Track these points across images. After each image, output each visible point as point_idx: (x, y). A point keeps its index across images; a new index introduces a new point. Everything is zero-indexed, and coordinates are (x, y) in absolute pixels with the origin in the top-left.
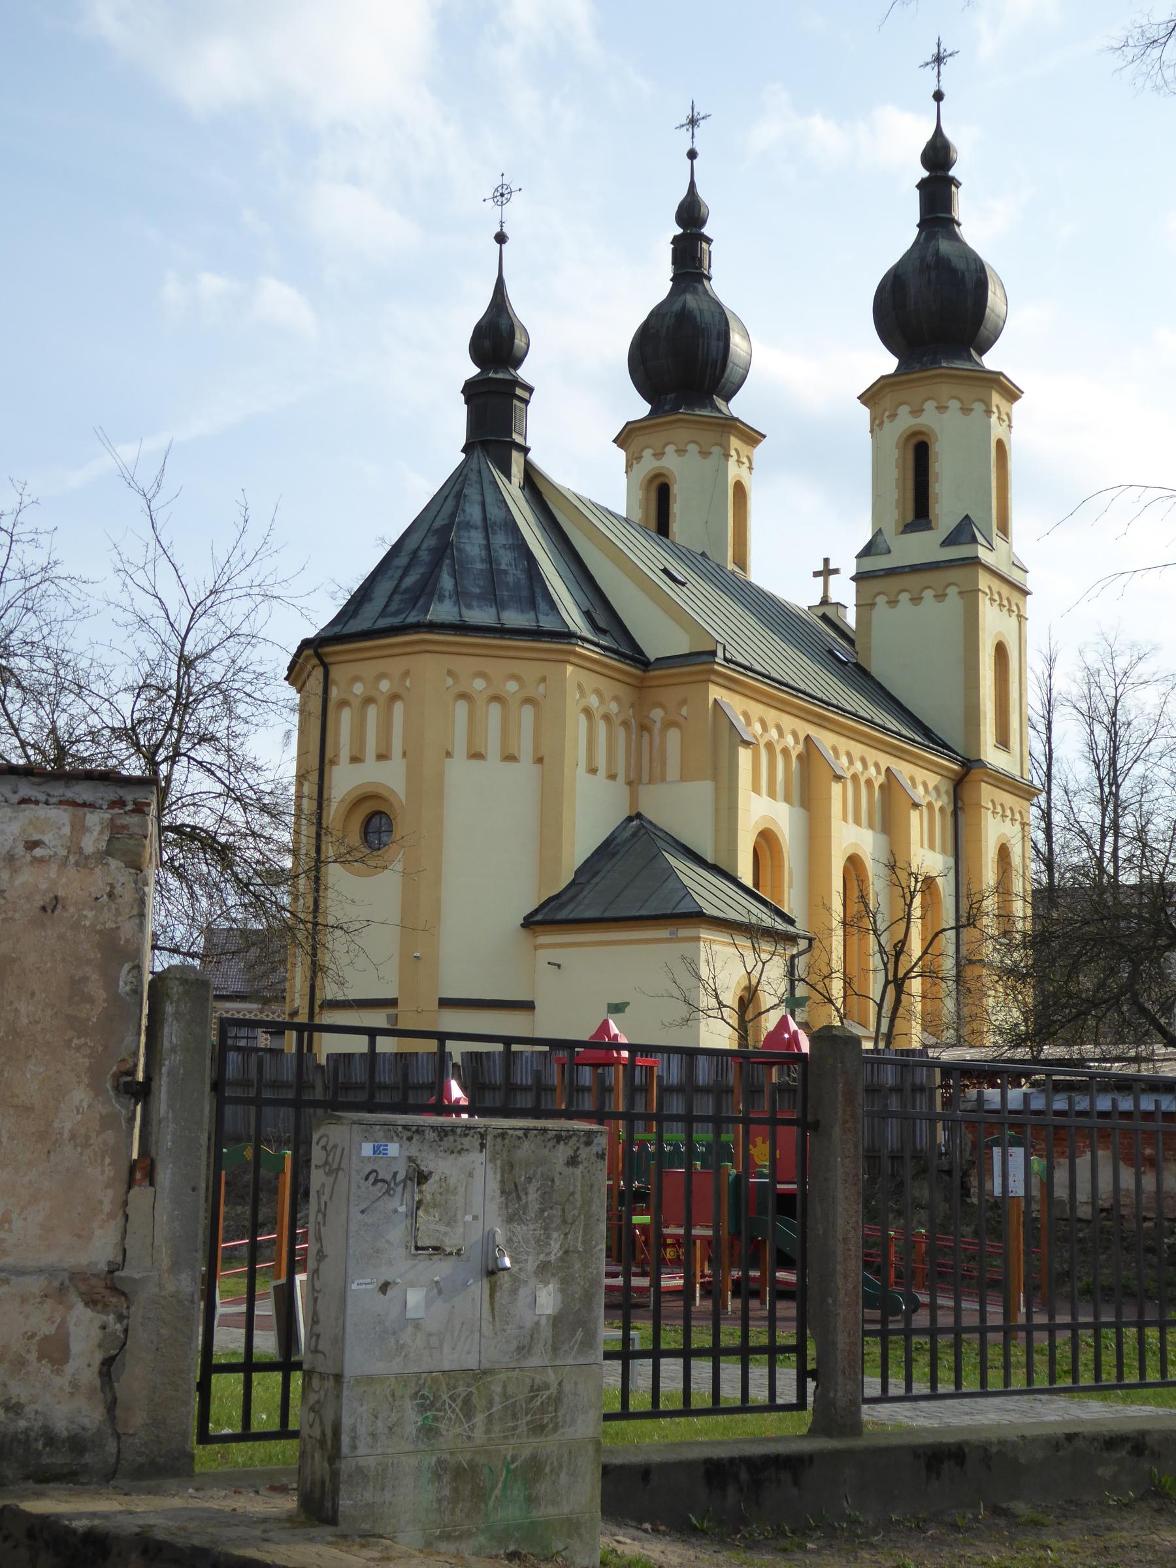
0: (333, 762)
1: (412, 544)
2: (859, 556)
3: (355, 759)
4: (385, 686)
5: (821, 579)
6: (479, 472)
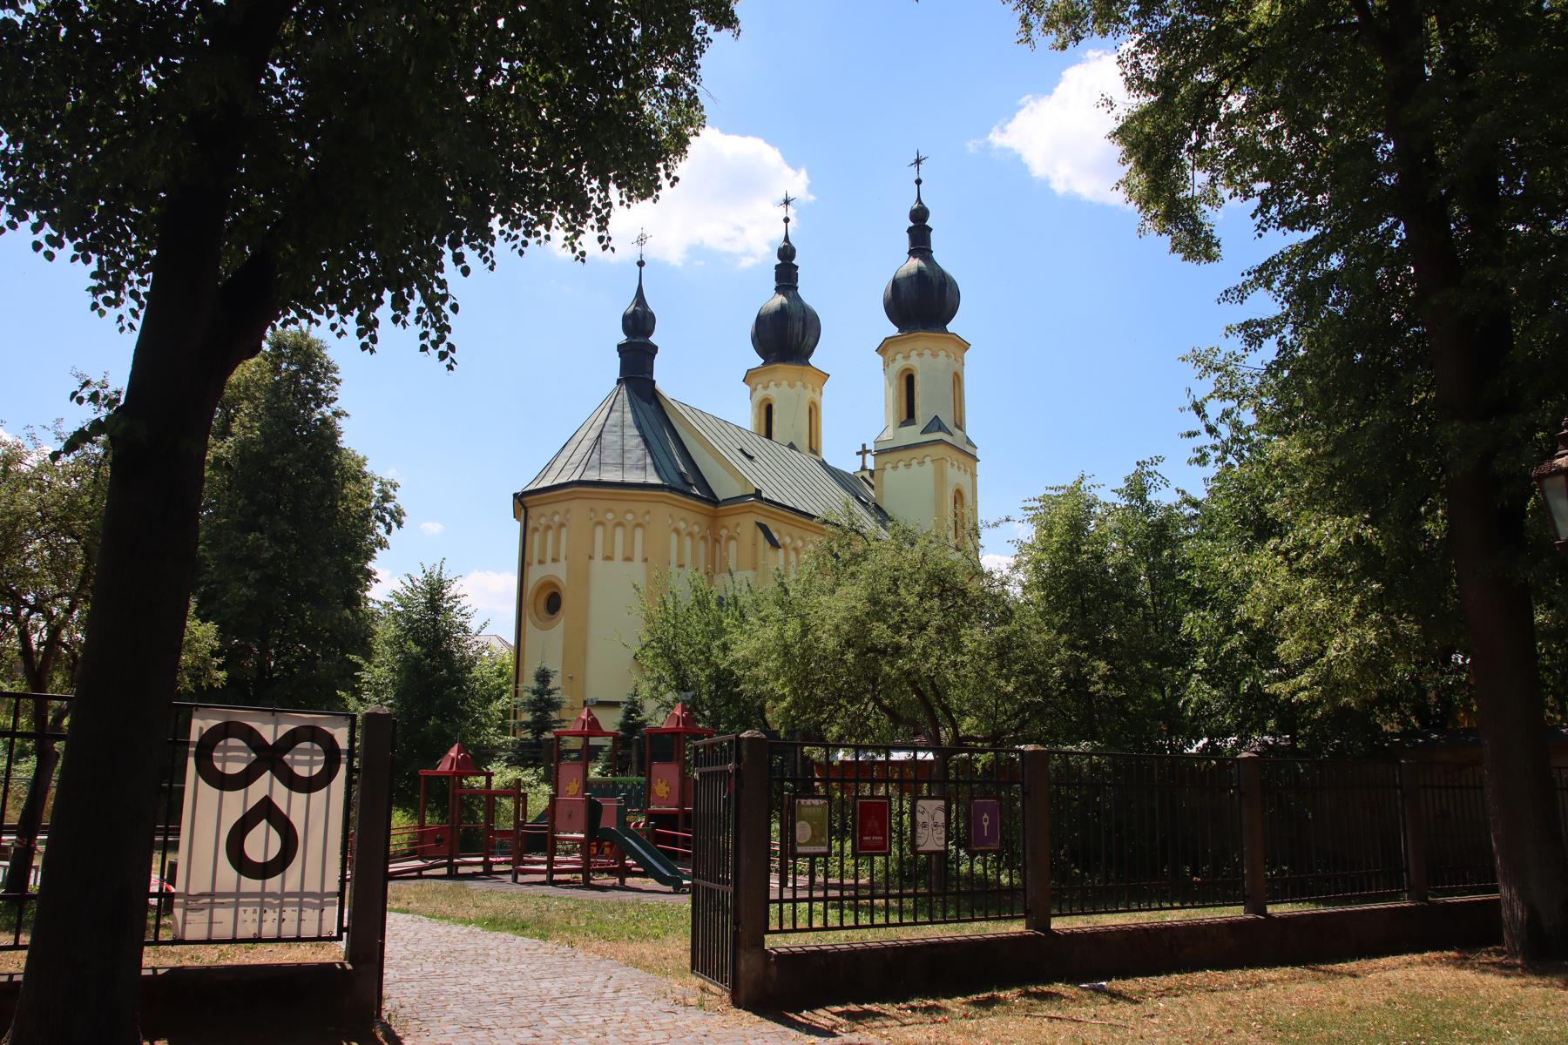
0: (529, 564)
3: (541, 562)
4: (557, 518)
5: (861, 456)
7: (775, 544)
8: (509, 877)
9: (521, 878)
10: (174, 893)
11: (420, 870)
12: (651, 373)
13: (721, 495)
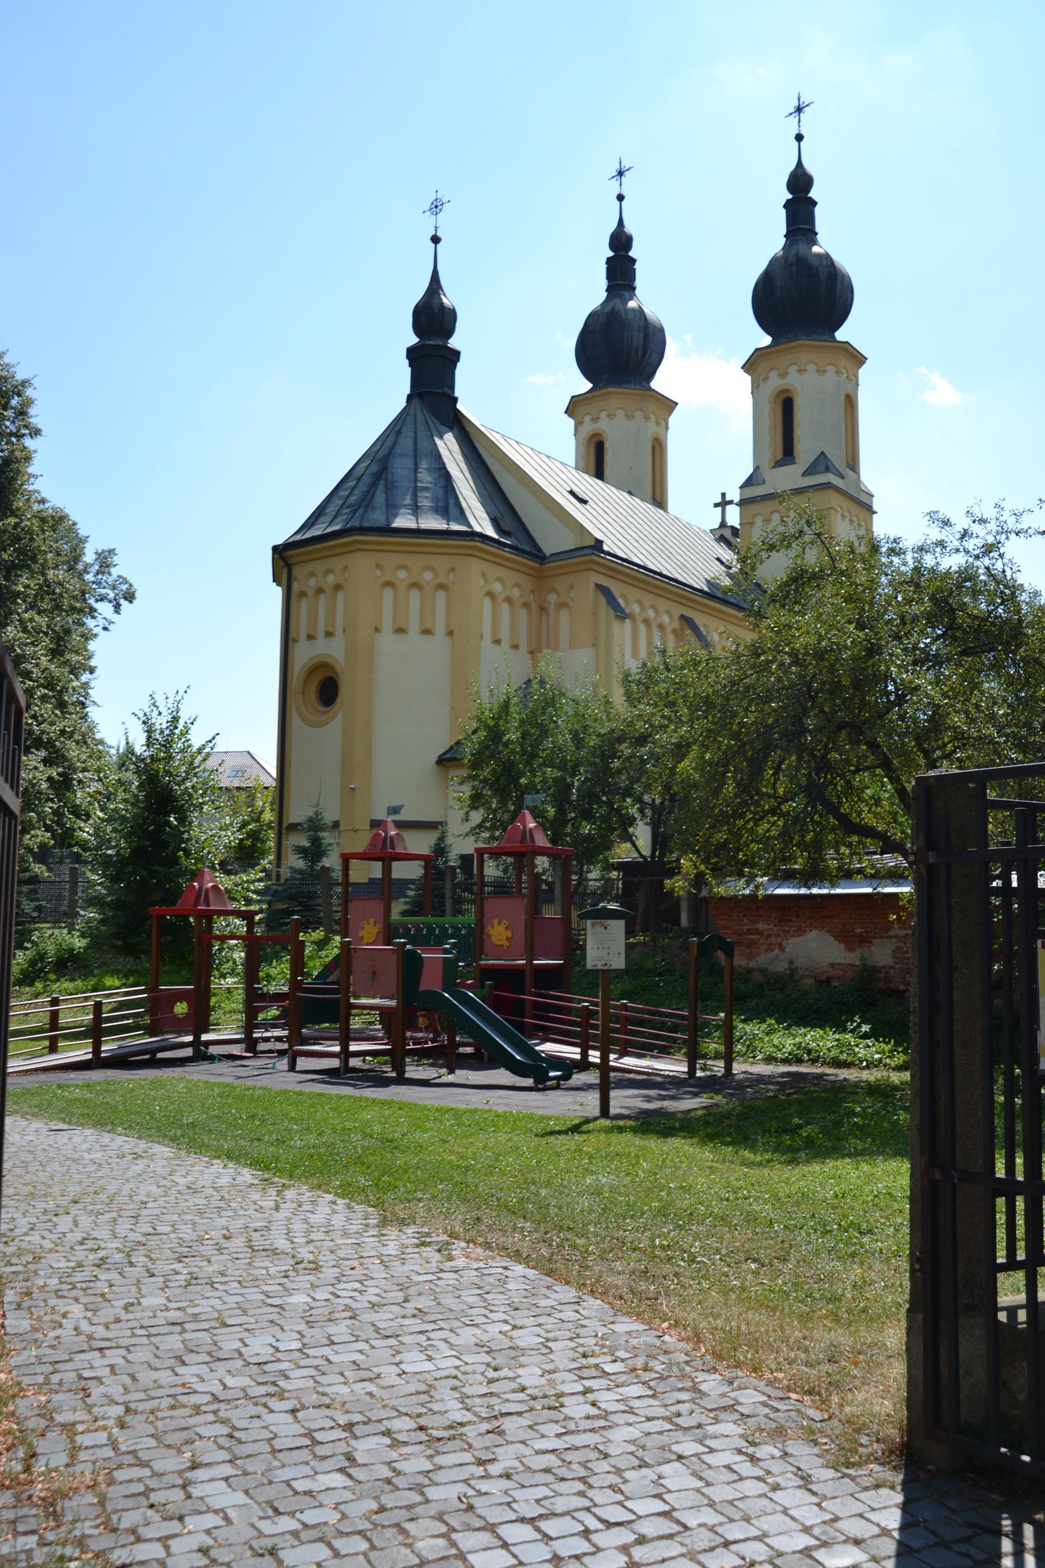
0: (295, 641)
1: (359, 471)
2: (742, 487)
5: (719, 509)
6: (415, 416)
7: (622, 615)
8: (283, 1063)
9: (302, 1063)
10: (731, 943)
11: (153, 1051)
12: (452, 387)
13: (549, 548)
